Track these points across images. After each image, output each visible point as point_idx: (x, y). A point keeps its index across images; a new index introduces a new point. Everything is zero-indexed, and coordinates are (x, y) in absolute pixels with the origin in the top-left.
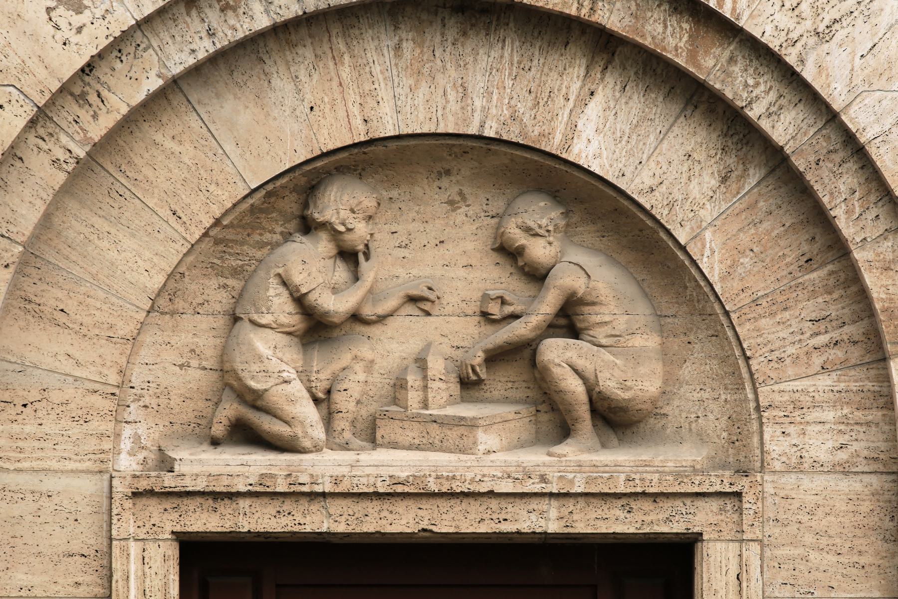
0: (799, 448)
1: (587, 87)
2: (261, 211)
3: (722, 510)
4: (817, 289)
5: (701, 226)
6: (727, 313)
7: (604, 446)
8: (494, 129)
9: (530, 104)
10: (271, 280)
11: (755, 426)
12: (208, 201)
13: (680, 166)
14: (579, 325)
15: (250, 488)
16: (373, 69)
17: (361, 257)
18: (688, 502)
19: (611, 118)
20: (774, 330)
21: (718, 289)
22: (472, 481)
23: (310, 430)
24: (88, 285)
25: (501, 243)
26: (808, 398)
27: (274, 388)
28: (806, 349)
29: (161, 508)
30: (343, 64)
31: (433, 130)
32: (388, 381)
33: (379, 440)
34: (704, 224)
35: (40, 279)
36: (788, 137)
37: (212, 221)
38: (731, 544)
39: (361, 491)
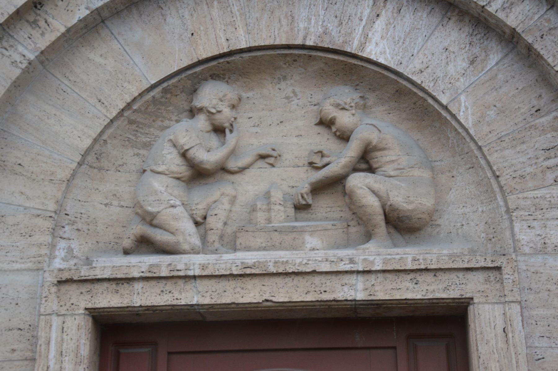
0: (543, 237)
1: (374, 12)
2: (161, 103)
3: (487, 281)
4: (546, 128)
5: (457, 92)
6: (480, 148)
7: (395, 246)
8: (312, 40)
9: (336, 24)
10: (165, 144)
11: (507, 224)
12: (123, 93)
13: (440, 56)
14: (375, 166)
15: (142, 274)
16: (233, 9)
17: (227, 131)
18: (461, 274)
19: (391, 29)
20: (516, 157)
21: (472, 132)
22: (300, 264)
23: (188, 238)
24: (39, 147)
25: (321, 119)
26: (546, 202)
27: (164, 211)
28: (541, 168)
29: (78, 292)
30: (213, 7)
31: (272, 43)
32: (245, 210)
33: (238, 246)
34: (460, 91)
35: (6, 145)
36: (518, 22)
37: (124, 105)
38: (496, 305)
39: (221, 274)
